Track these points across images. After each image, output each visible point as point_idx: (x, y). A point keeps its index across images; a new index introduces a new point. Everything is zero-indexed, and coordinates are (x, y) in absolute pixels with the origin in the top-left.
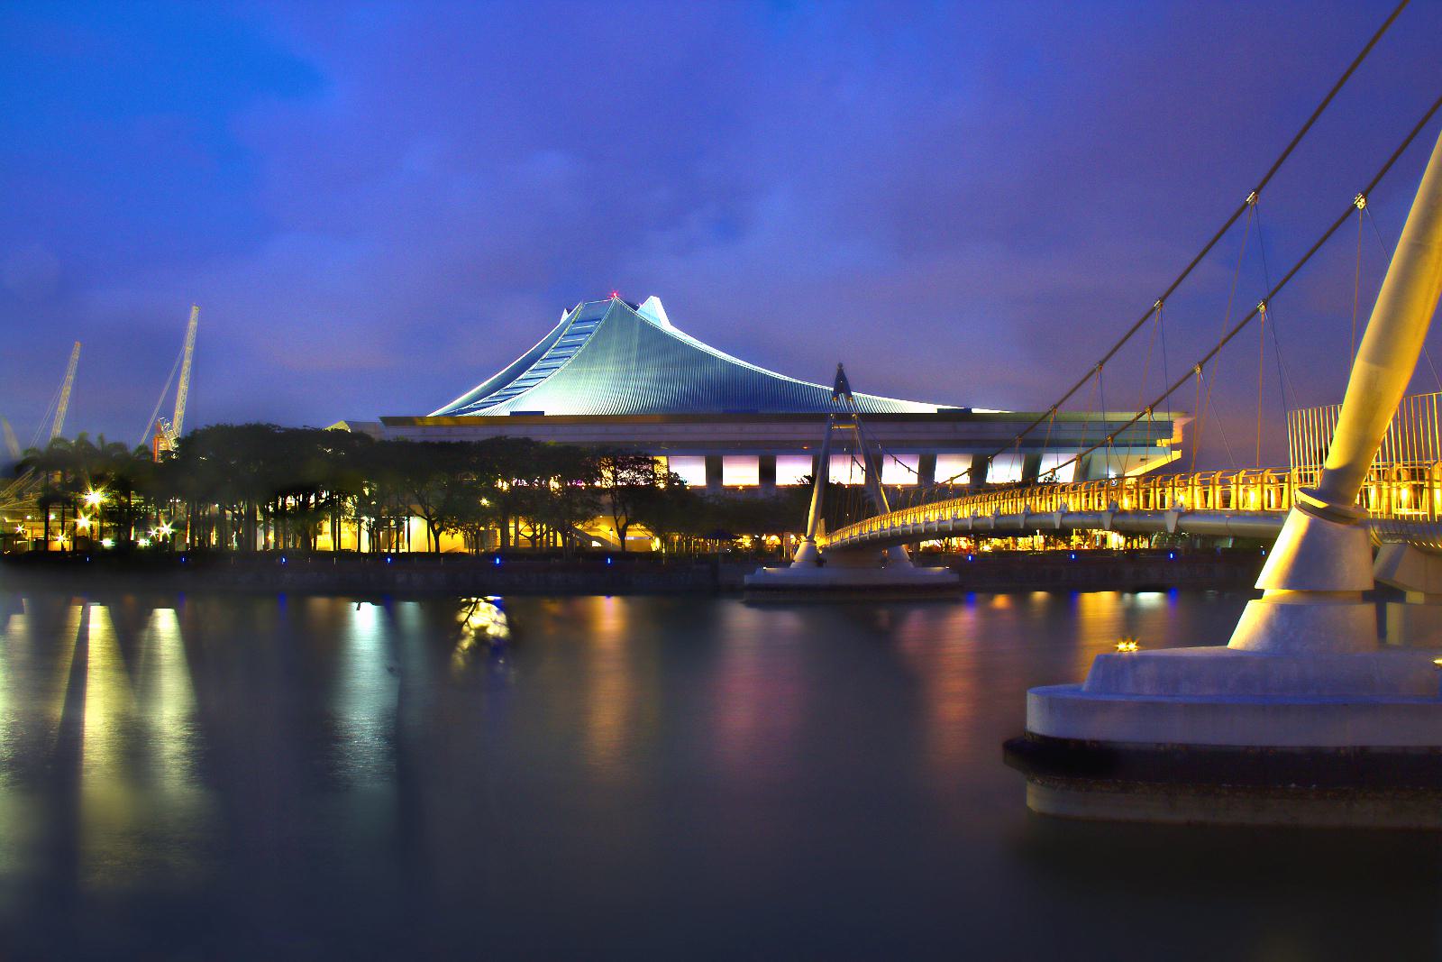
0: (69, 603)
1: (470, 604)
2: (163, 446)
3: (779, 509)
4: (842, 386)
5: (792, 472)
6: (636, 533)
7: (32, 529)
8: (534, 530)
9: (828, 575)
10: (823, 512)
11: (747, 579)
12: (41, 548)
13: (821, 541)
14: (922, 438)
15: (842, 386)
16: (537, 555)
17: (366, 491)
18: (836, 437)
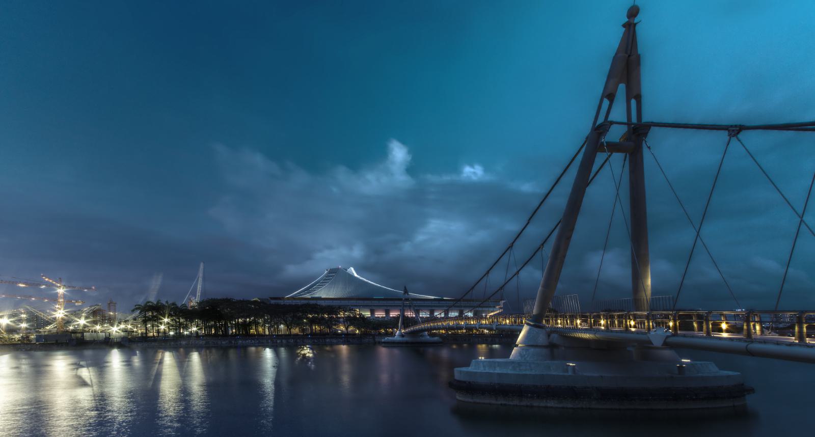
0: (156, 352)
1: (301, 348)
2: (192, 304)
3: (393, 323)
4: (406, 292)
5: (393, 314)
6: (351, 328)
7: (141, 329)
8: (321, 328)
9: (405, 339)
10: (403, 323)
11: (383, 340)
12: (145, 335)
13: (403, 331)
14: (431, 306)
15: (406, 292)
16: (322, 335)
17: (266, 318)
18: (405, 304)
